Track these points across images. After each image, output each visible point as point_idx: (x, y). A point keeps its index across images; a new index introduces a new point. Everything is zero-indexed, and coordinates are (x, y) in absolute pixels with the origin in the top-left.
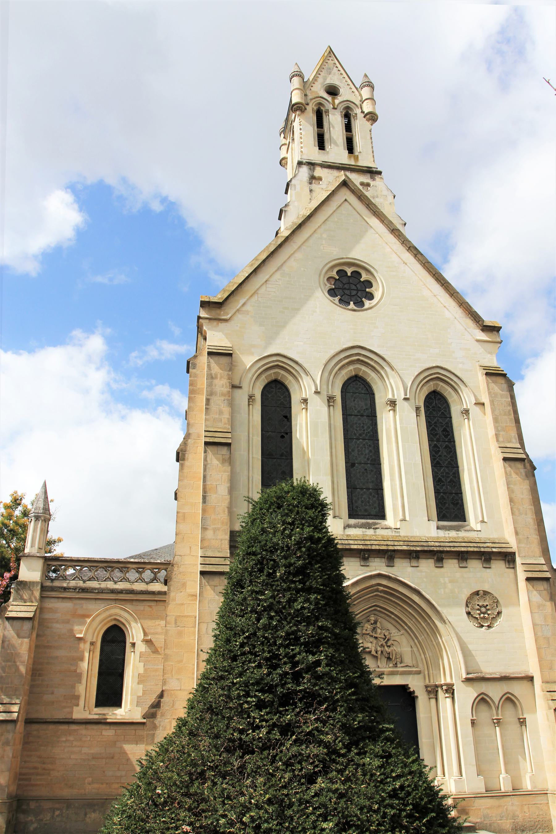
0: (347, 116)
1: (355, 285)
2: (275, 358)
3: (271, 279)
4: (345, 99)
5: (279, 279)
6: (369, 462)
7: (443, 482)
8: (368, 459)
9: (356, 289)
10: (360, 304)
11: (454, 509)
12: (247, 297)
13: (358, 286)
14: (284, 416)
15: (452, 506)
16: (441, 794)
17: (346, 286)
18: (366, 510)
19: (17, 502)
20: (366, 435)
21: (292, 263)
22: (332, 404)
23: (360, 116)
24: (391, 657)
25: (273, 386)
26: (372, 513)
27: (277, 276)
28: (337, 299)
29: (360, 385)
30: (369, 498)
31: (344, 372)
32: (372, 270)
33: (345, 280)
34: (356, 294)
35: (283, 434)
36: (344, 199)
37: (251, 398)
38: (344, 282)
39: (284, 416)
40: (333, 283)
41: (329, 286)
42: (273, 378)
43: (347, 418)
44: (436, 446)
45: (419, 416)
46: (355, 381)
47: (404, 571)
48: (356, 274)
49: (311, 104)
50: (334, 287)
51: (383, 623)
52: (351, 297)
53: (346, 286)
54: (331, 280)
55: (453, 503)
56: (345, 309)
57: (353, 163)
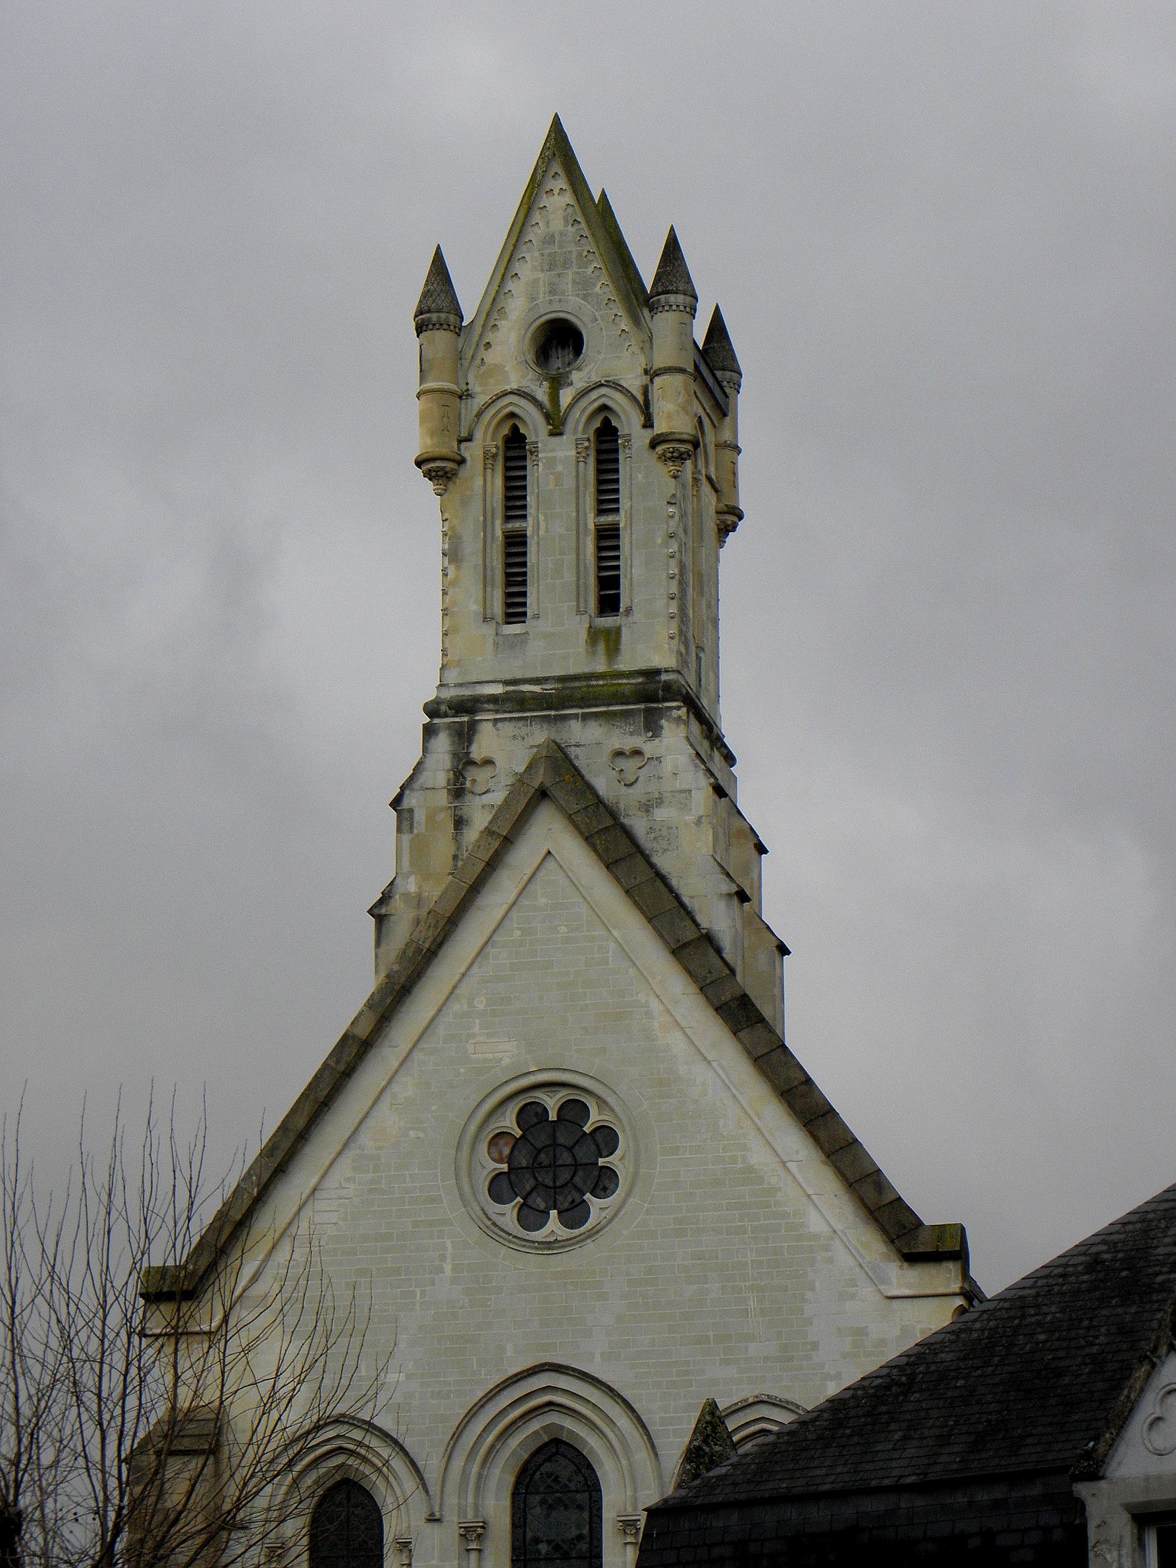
0: (606, 441)
3: (329, 1183)
4: (595, 379)
5: (348, 1180)
12: (261, 1257)
19: (437, 308)
21: (388, 1119)
22: (473, 1546)
27: (345, 1168)
28: (595, 1117)
31: (514, 1442)
33: (541, 1139)
36: (544, 852)
41: (492, 1166)
48: (575, 1110)
49: (479, 435)
50: (504, 1167)
52: (553, 1195)
57: (601, 667)
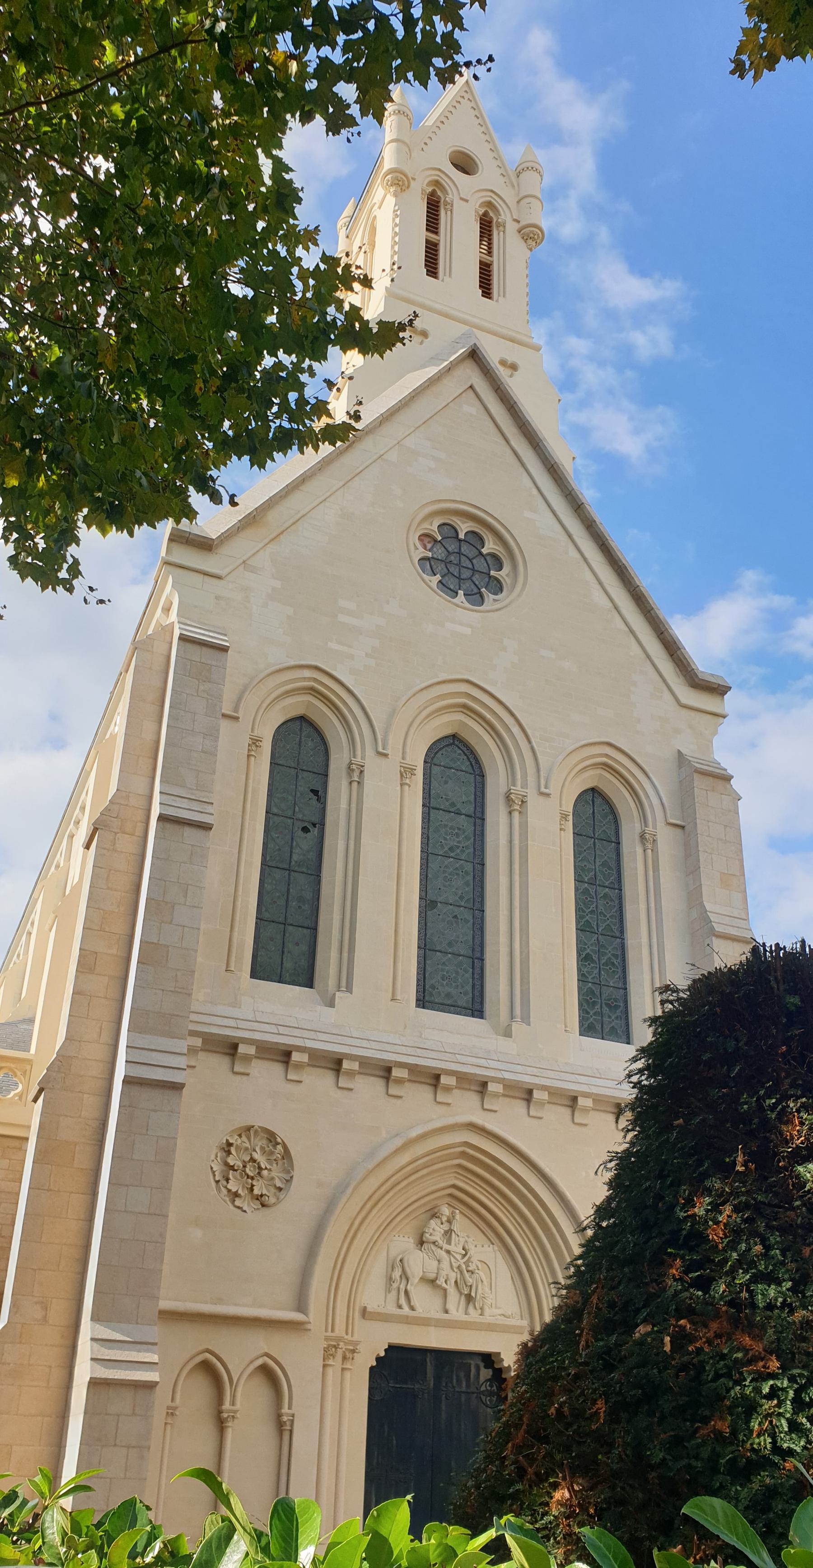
1: (471, 560)
2: (307, 673)
6: (463, 904)
7: (593, 961)
8: (461, 898)
9: (470, 566)
10: (476, 598)
11: (610, 1017)
13: (474, 561)
14: (312, 791)
15: (606, 1010)
16: (222, 467)
17: (452, 558)
18: (448, 995)
20: (463, 851)
23: (511, 228)
24: (473, 1294)
25: (298, 723)
26: (460, 1003)
29: (460, 754)
30: (457, 973)
32: (521, 579)
34: (470, 578)
35: (306, 824)
37: (255, 742)
38: (450, 549)
39: (312, 791)
40: (429, 546)
42: (300, 712)
43: (429, 814)
44: (586, 892)
45: (564, 830)
46: (451, 744)
47: (508, 1120)
48: (475, 538)
51: (467, 1234)
53: (452, 558)
54: (426, 540)
55: (608, 1005)
56: (450, 602)
